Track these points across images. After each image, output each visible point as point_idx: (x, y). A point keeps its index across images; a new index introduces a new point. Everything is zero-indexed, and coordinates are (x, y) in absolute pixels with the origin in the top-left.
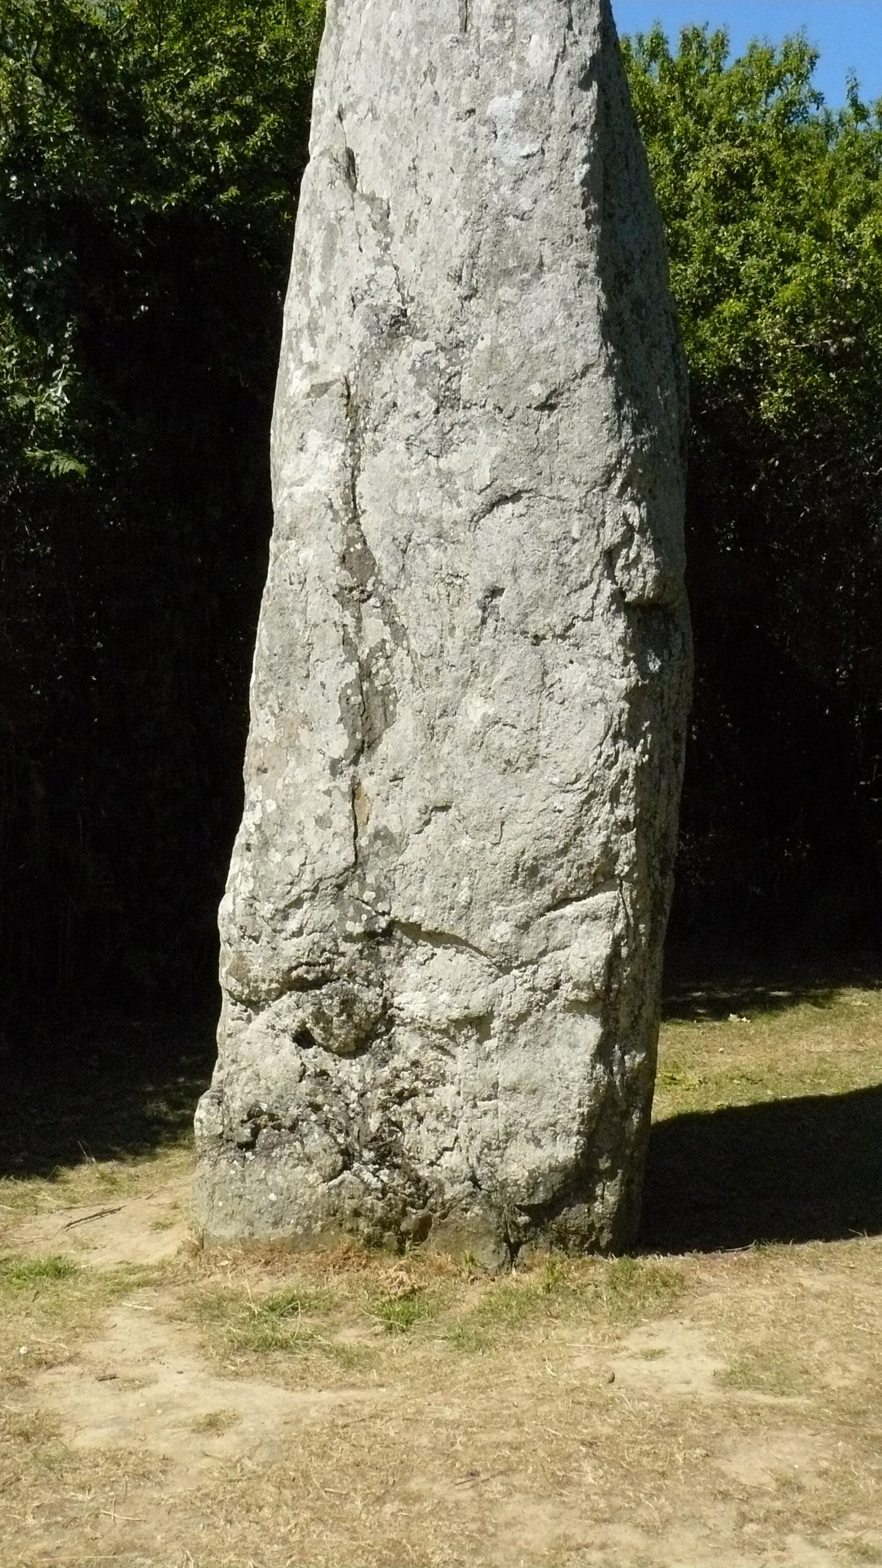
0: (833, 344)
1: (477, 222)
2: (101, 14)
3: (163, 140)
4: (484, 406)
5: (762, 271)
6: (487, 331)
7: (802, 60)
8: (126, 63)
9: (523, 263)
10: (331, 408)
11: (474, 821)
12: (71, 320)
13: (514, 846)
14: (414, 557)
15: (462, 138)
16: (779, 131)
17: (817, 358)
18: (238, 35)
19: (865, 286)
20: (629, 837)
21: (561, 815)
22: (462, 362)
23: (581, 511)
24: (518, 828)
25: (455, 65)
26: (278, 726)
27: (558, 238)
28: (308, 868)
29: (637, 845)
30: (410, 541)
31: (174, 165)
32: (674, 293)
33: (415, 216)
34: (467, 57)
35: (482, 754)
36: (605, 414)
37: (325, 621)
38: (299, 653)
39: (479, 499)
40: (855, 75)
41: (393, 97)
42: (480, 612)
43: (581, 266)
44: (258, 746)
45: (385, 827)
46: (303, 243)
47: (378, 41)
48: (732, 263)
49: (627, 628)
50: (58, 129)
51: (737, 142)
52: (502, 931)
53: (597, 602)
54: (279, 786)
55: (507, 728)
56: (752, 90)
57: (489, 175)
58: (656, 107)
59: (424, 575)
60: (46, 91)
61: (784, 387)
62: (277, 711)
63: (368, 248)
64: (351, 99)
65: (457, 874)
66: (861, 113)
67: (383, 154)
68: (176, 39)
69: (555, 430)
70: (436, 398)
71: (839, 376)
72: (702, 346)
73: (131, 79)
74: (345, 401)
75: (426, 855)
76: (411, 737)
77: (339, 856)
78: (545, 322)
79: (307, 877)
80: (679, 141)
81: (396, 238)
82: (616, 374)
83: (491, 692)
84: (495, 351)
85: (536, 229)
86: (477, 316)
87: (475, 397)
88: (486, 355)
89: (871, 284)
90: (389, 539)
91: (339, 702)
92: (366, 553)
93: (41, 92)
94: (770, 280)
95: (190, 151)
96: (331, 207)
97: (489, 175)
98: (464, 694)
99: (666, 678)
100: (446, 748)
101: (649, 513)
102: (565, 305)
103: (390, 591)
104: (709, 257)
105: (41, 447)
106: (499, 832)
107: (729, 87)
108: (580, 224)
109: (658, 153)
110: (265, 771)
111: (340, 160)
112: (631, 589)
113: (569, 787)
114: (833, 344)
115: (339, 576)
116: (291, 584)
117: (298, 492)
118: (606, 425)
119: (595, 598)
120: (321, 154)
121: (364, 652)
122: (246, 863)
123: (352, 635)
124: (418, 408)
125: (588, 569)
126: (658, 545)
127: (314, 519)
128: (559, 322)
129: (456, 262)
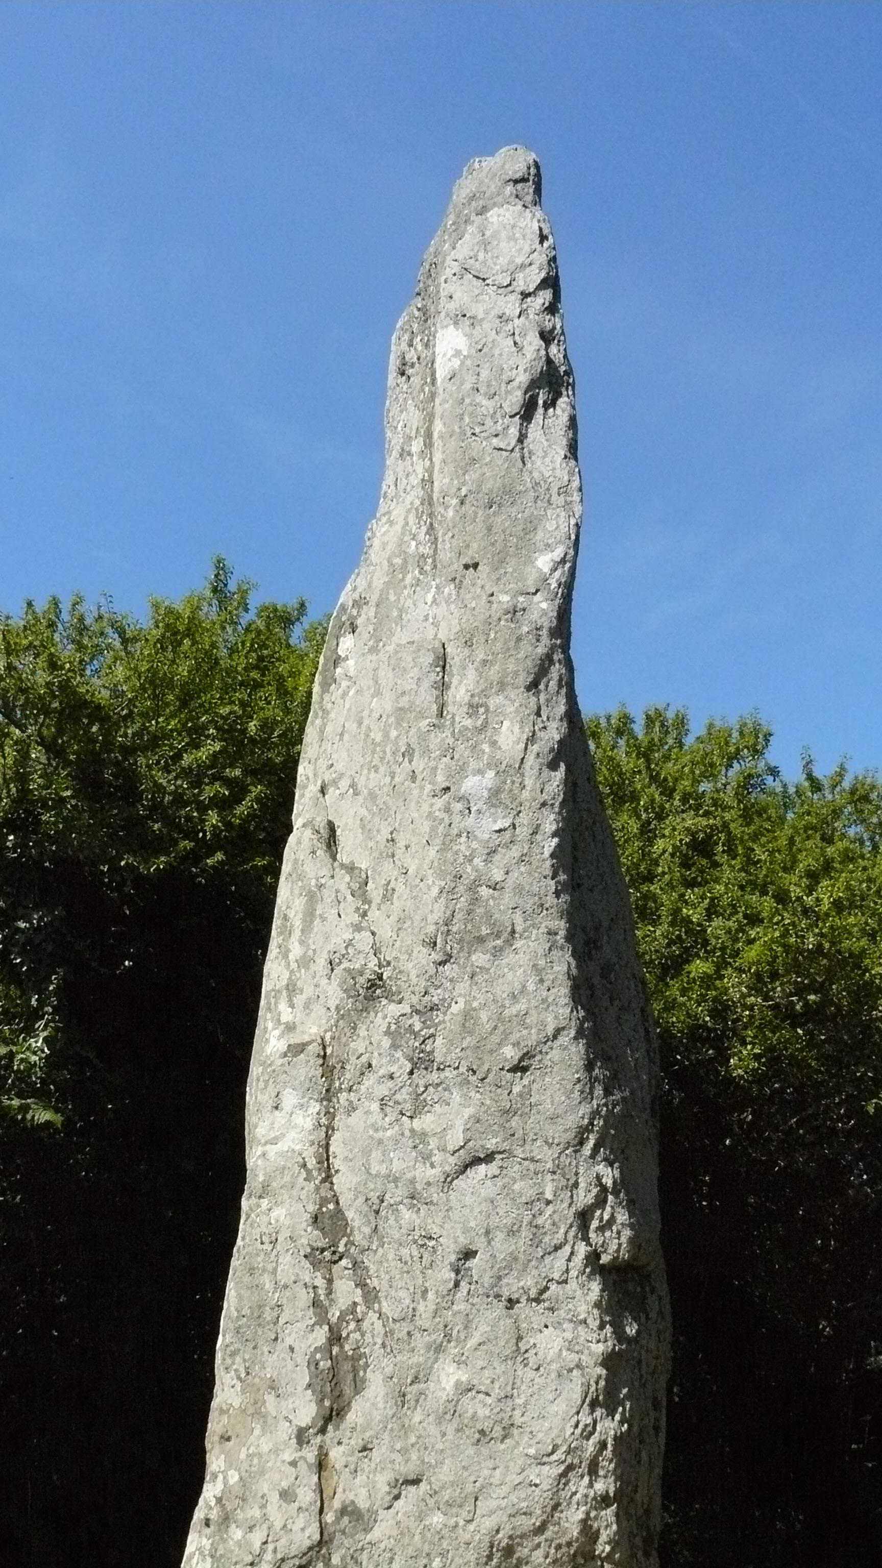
0: (799, 1001)
1: (452, 891)
2: (106, 694)
3: (156, 808)
4: (458, 1068)
5: (729, 932)
6: (460, 996)
7: (757, 737)
8: (125, 735)
9: (496, 929)
10: (307, 1068)
11: (446, 1495)
12: (57, 973)
13: (488, 1524)
14: (387, 1217)
15: (437, 813)
16: (740, 801)
17: (785, 1014)
18: (230, 713)
19: (827, 945)
20: (609, 1513)
21: (537, 1490)
22: (437, 1025)
23: (554, 1173)
24: (493, 1504)
25: (431, 747)
26: (243, 1391)
27: (528, 907)
28: (270, 1547)
29: (618, 1522)
30: (382, 1201)
31: (165, 831)
32: (644, 954)
33: (392, 885)
34: (443, 740)
35: (454, 1424)
36: (576, 1076)
37: (295, 1282)
38: (268, 1315)
39: (452, 1160)
40: (810, 752)
41: (373, 775)
42: (453, 1275)
43: (551, 933)
44: (222, 1412)
45: (353, 1502)
46: (284, 908)
47: (360, 724)
48: (699, 925)
49: (602, 1290)
50: (57, 794)
51: (701, 812)
53: (571, 1264)
54: (243, 1456)
55: (481, 1396)
56: (712, 765)
57: (463, 848)
58: (624, 780)
59: (397, 1236)
60: (48, 759)
61: (754, 1044)
62: (243, 1375)
63: (347, 914)
64: (334, 776)
65: (428, 1555)
66: (816, 786)
67: (363, 827)
68: (173, 716)
69: (527, 1092)
70: (411, 1060)
71: (808, 1032)
72: (671, 1005)
73: (129, 751)
74: (321, 1061)
75: (395, 1532)
76: (381, 1405)
78: (517, 986)
80: (646, 810)
81: (374, 906)
82: (586, 1037)
83: (464, 1358)
84: (468, 1014)
85: (508, 898)
86: (451, 981)
87: (449, 1058)
88: (460, 1018)
89: (833, 944)
90: (361, 1199)
91: (308, 1367)
92: (339, 1213)
93: (43, 760)
94: (736, 940)
95: (180, 818)
96: (311, 875)
97: (463, 848)
98: (436, 1360)
99: (644, 1342)
100: (417, 1418)
101: (621, 1173)
102: (537, 970)
103: (362, 1252)
104: (677, 919)
105: (19, 1096)
106: (472, 1508)
107: (692, 762)
108: (550, 893)
109: (625, 823)
110: (228, 1439)
111: (322, 831)
112: (605, 1252)
113: (545, 1459)
114: (799, 1001)
115: (311, 1237)
116: (262, 1243)
117: (272, 1150)
118: (578, 1087)
119: (569, 1260)
120: (304, 826)
121: (334, 1315)
122: (204, 1541)
123: (322, 1298)
124: (393, 1069)
125: (562, 1231)
126: (632, 1206)
127: (287, 1178)
128: (531, 987)
129: (431, 929)
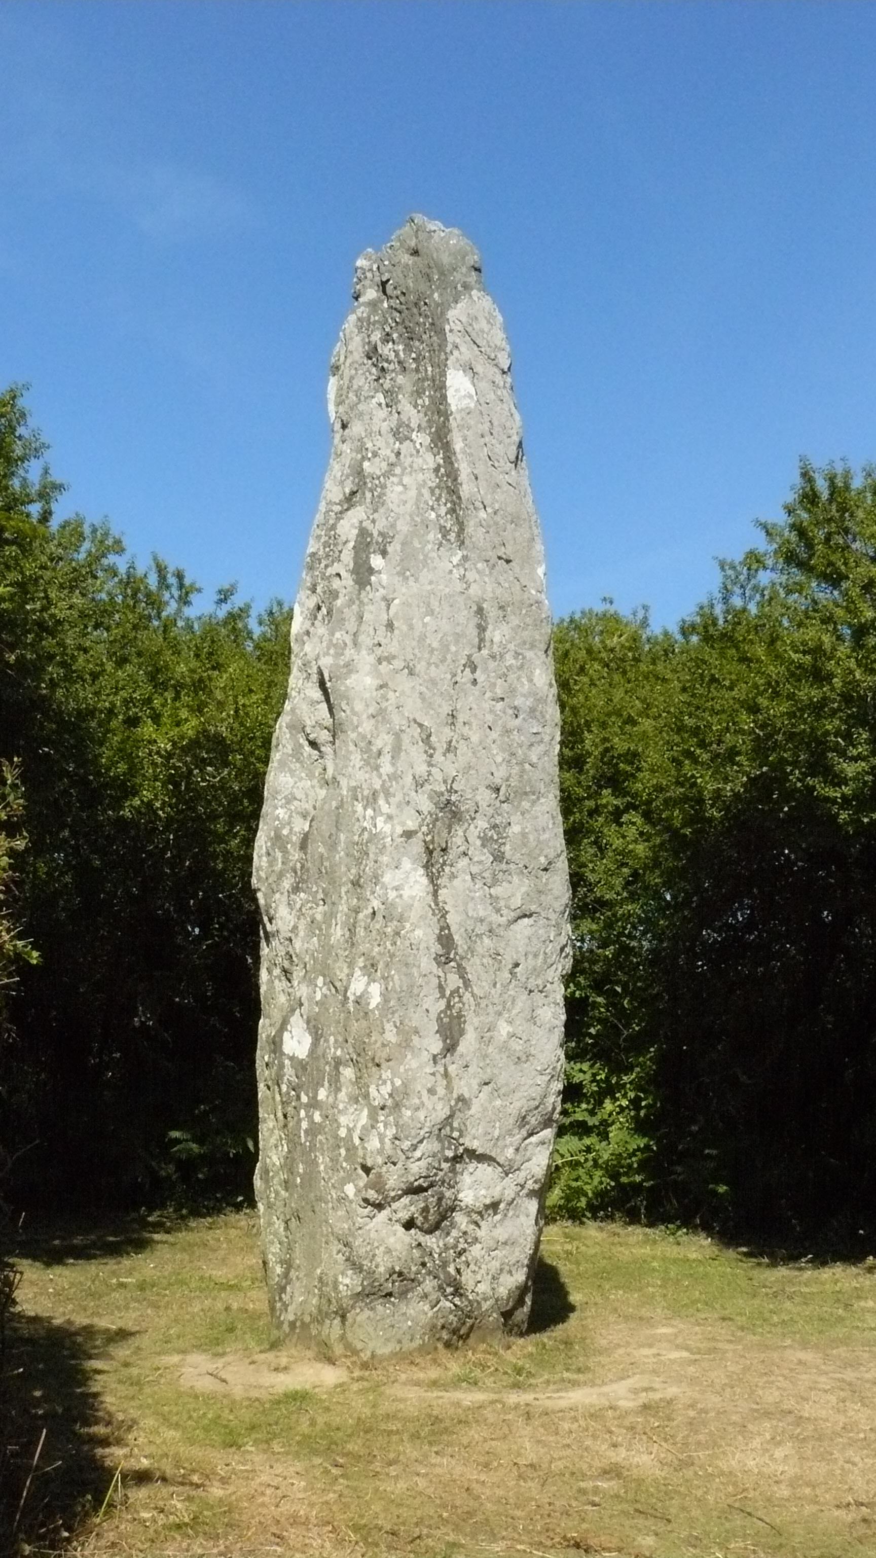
1: (509, 762)
11: (502, 1091)
13: (518, 1104)
24: (520, 1094)
26: (398, 1034)
38: (416, 991)
77: (442, 1112)
79: (428, 1124)
90: (463, 930)
92: (450, 937)
115: (437, 948)
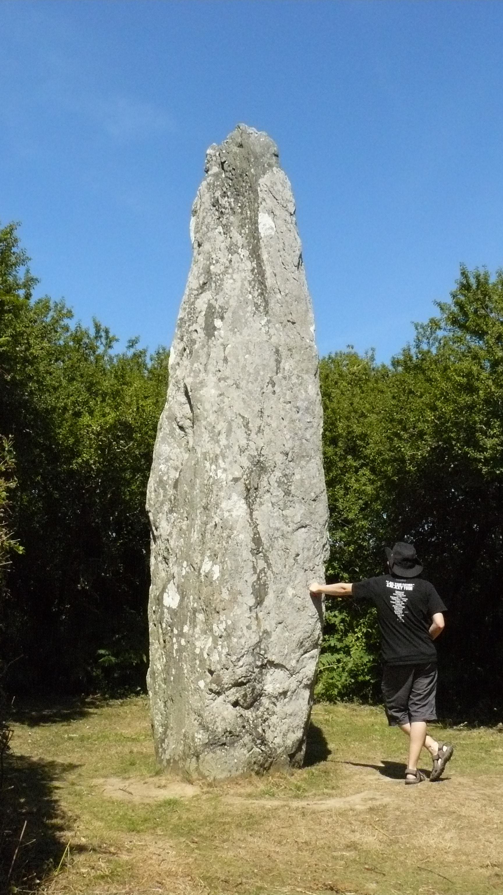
11: (290, 627)
13: (298, 635)
24: (300, 629)
26: (229, 594)
38: (239, 570)
52: (293, 663)
77: (255, 639)
79: (246, 646)
84: (302, 480)
92: (259, 539)
115: (252, 545)
124: (279, 494)
